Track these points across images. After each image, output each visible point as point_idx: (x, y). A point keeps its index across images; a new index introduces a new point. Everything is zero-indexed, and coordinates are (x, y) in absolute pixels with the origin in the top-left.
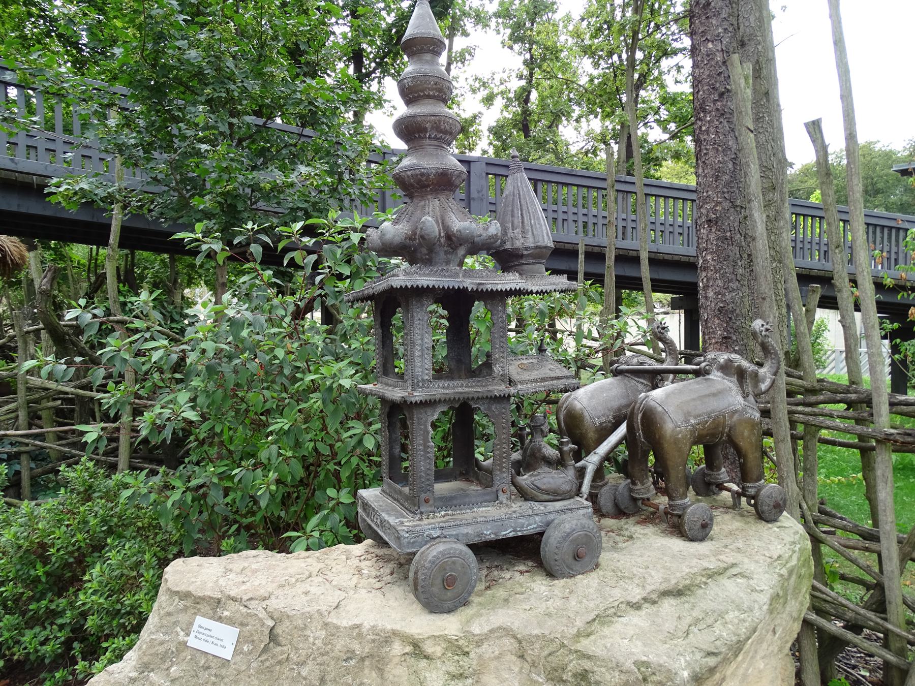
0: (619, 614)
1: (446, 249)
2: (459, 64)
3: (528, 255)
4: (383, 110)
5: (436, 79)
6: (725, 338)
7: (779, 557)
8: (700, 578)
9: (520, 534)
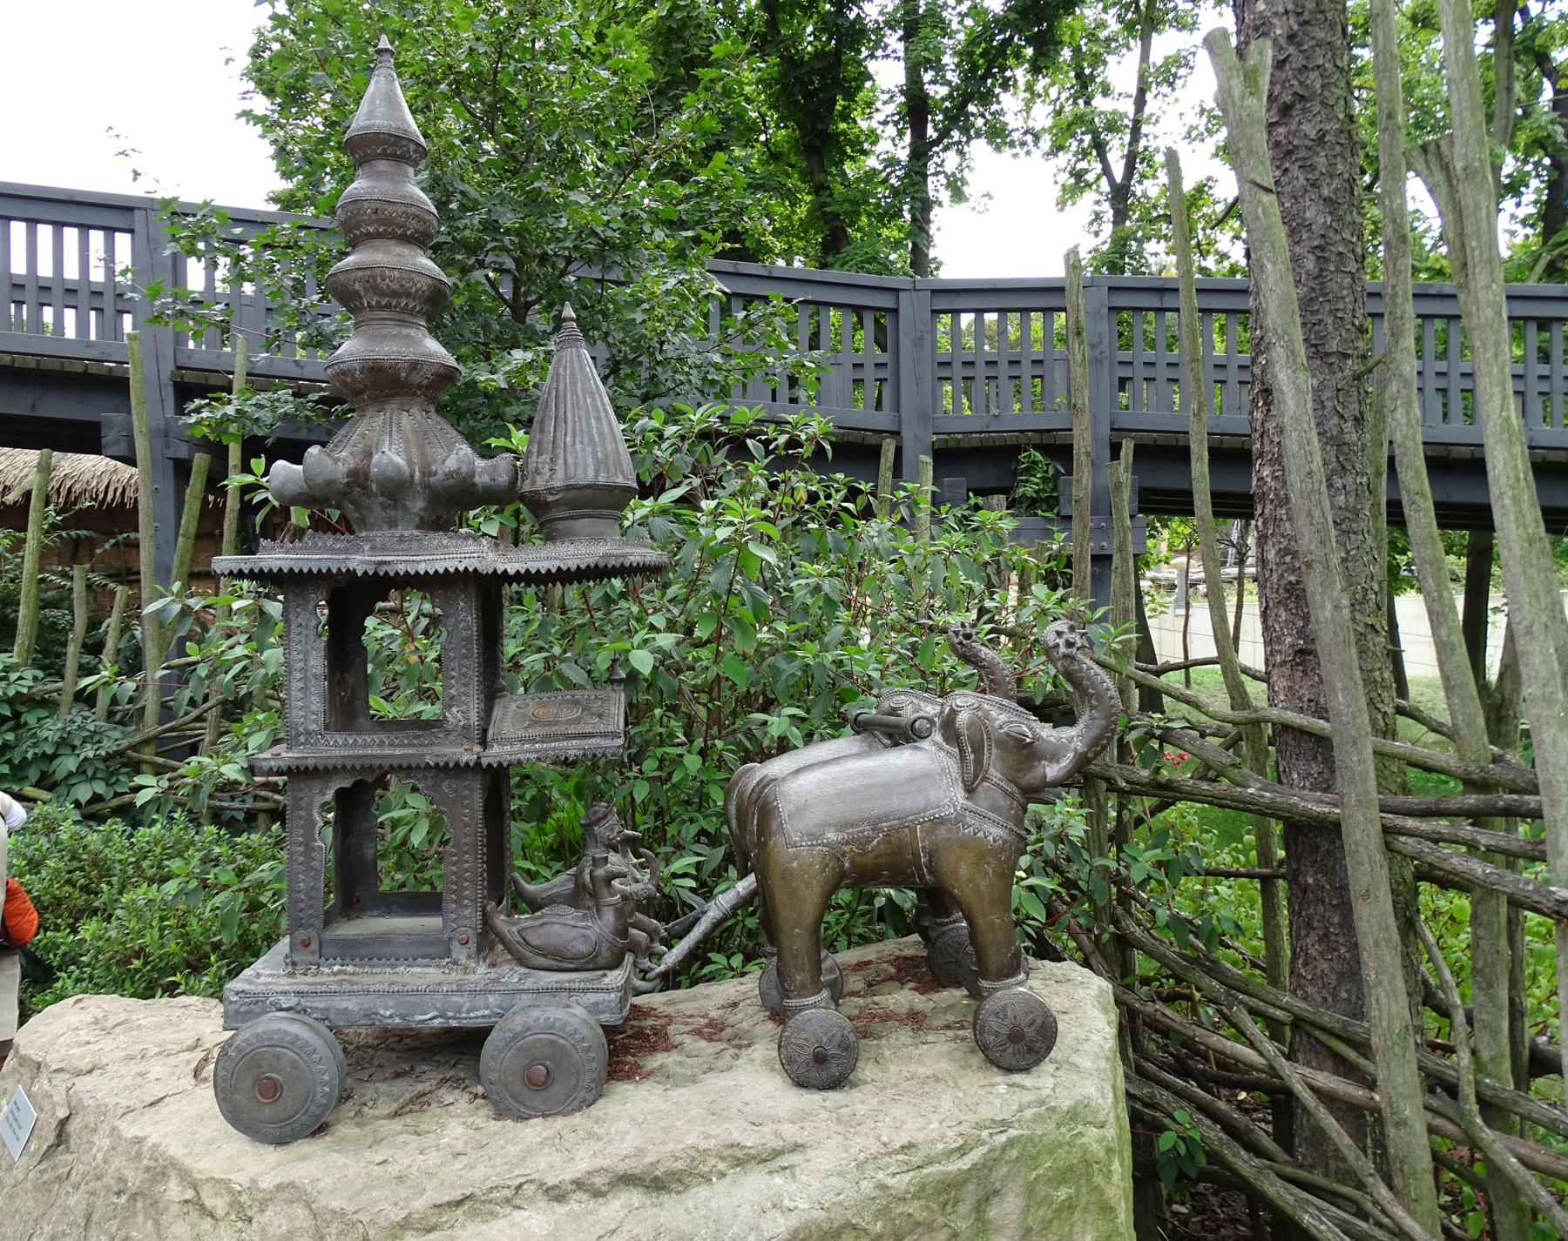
0: (518, 1202)
1: (381, 499)
2: (1165, 89)
3: (557, 503)
4: (971, 203)
5: (374, 205)
6: (1301, 652)
7: (908, 1147)
8: (713, 1162)
9: (454, 1023)
